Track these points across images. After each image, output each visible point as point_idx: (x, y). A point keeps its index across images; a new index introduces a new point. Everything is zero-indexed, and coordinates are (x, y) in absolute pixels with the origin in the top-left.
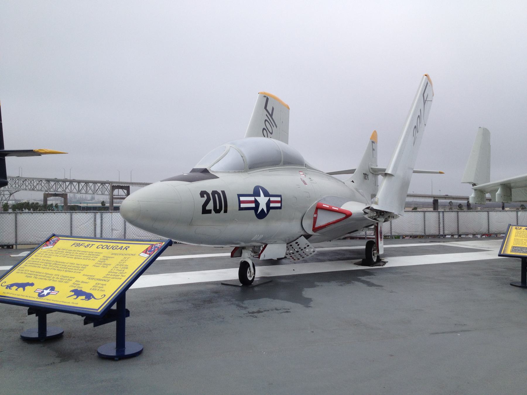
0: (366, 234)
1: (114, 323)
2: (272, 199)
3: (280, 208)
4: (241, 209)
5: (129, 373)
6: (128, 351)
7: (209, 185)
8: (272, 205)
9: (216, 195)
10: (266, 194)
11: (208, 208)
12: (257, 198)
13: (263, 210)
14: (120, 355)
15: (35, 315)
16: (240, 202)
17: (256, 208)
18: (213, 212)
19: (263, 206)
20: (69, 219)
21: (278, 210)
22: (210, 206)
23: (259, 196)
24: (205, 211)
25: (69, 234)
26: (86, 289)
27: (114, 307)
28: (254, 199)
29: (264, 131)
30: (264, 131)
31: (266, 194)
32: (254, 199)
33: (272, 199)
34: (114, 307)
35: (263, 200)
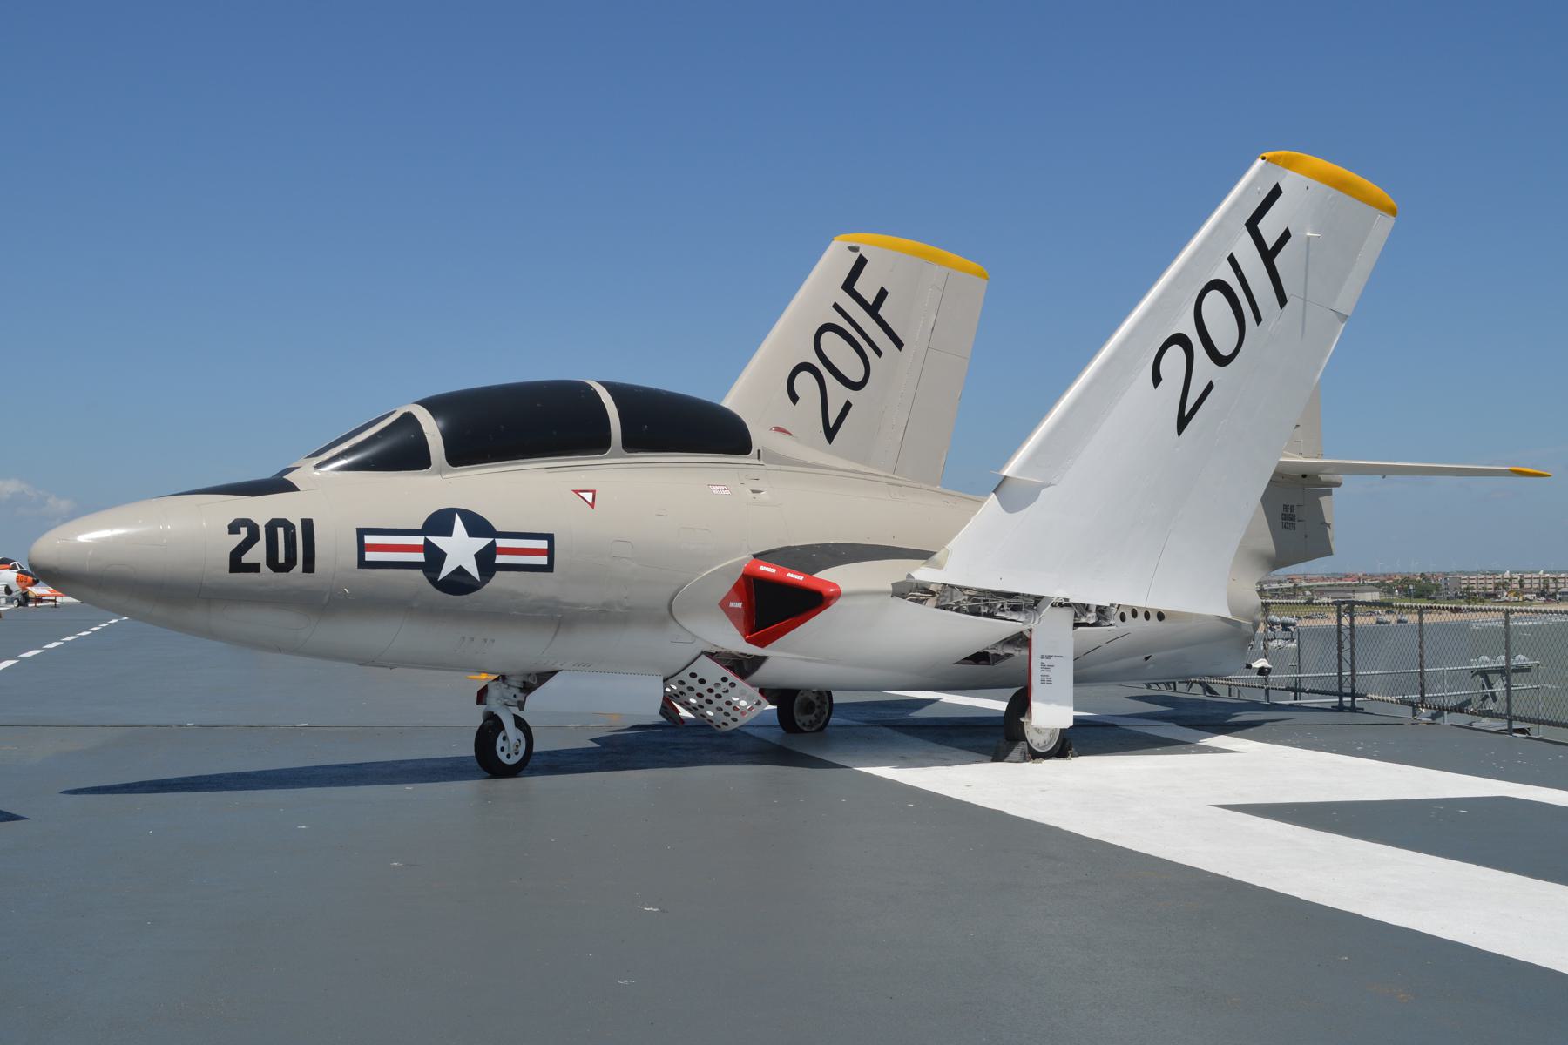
2: (500, 543)
4: (363, 564)
7: (262, 510)
8: (500, 559)
9: (281, 531)
10: (477, 526)
11: (247, 558)
16: (362, 548)
18: (264, 568)
22: (257, 553)
31: (477, 526)
33: (500, 543)
35: (460, 549)
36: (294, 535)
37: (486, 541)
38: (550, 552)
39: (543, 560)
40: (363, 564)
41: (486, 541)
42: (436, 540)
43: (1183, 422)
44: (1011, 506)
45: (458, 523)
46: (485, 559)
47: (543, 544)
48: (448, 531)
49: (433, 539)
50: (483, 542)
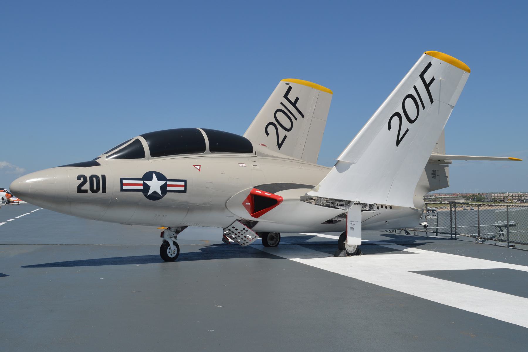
2: (168, 183)
4: (122, 190)
7: (88, 172)
8: (168, 188)
9: (94, 179)
10: (161, 177)
11: (83, 188)
16: (122, 184)
18: (89, 191)
22: (87, 186)
31: (161, 177)
33: (168, 183)
35: (155, 185)
36: (99, 180)
37: (164, 182)
38: (185, 186)
39: (183, 189)
40: (122, 190)
41: (164, 182)
42: (147, 182)
43: (398, 142)
44: (340, 170)
45: (154, 176)
46: (163, 188)
47: (183, 183)
48: (151, 179)
49: (146, 182)
50: (162, 183)
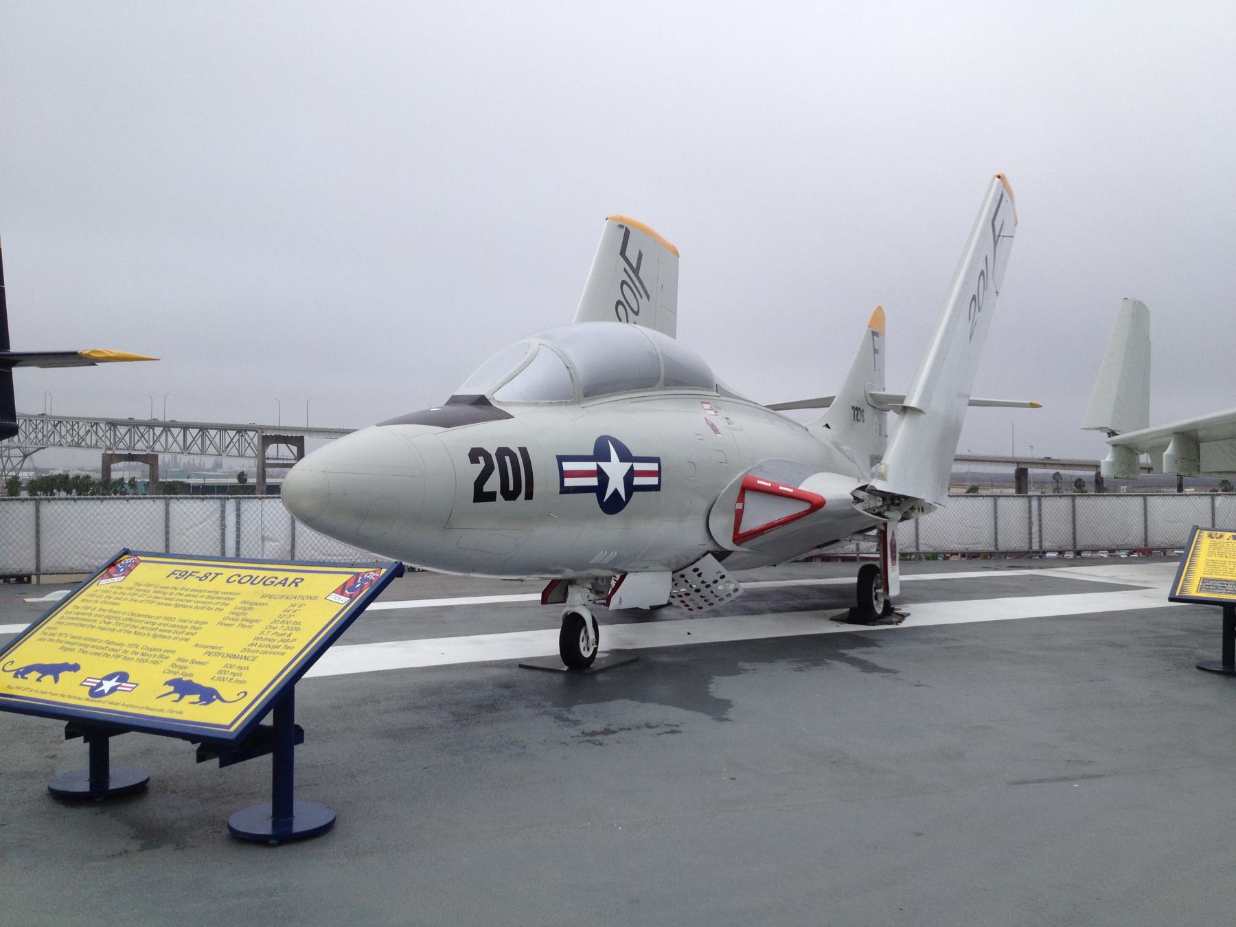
0: (858, 549)
1: (268, 758)
2: (638, 466)
3: (656, 488)
4: (565, 490)
5: (303, 874)
6: (301, 823)
7: (489, 435)
8: (638, 481)
9: (507, 458)
10: (625, 456)
11: (487, 488)
12: (602, 465)
13: (616, 492)
14: (283, 834)
15: (81, 739)
16: (563, 474)
17: (600, 489)
18: (499, 496)
19: (616, 483)
20: (162, 513)
21: (653, 493)
22: (493, 484)
23: (608, 459)
24: (481, 495)
25: (162, 550)
26: (202, 678)
27: (268, 721)
28: (595, 468)
29: (620, 307)
30: (620, 307)
31: (625, 456)
32: (595, 468)
33: (638, 466)
34: (268, 721)
35: (616, 470)
